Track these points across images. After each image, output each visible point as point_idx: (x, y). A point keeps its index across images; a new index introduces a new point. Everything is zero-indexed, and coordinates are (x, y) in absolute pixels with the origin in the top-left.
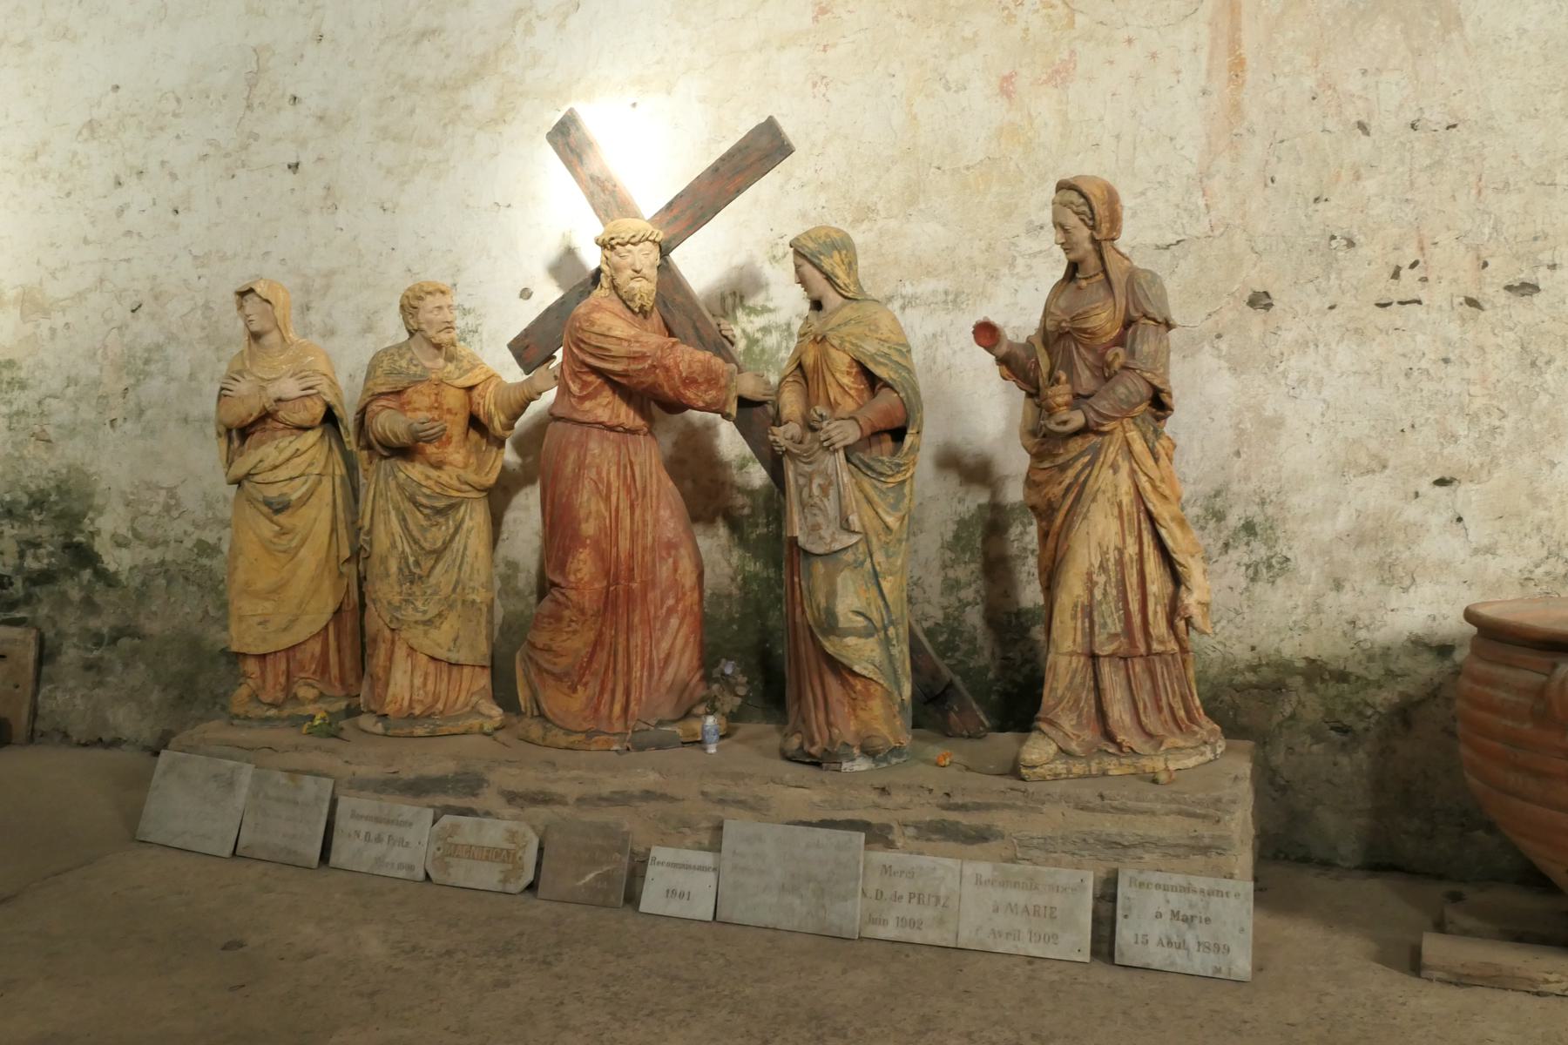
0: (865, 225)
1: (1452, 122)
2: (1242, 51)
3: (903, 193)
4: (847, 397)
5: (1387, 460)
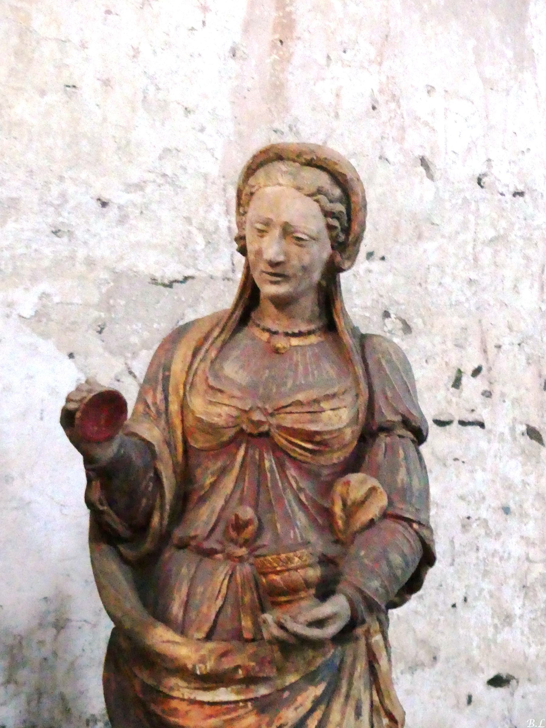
1: (521, 188)
5: (437, 649)
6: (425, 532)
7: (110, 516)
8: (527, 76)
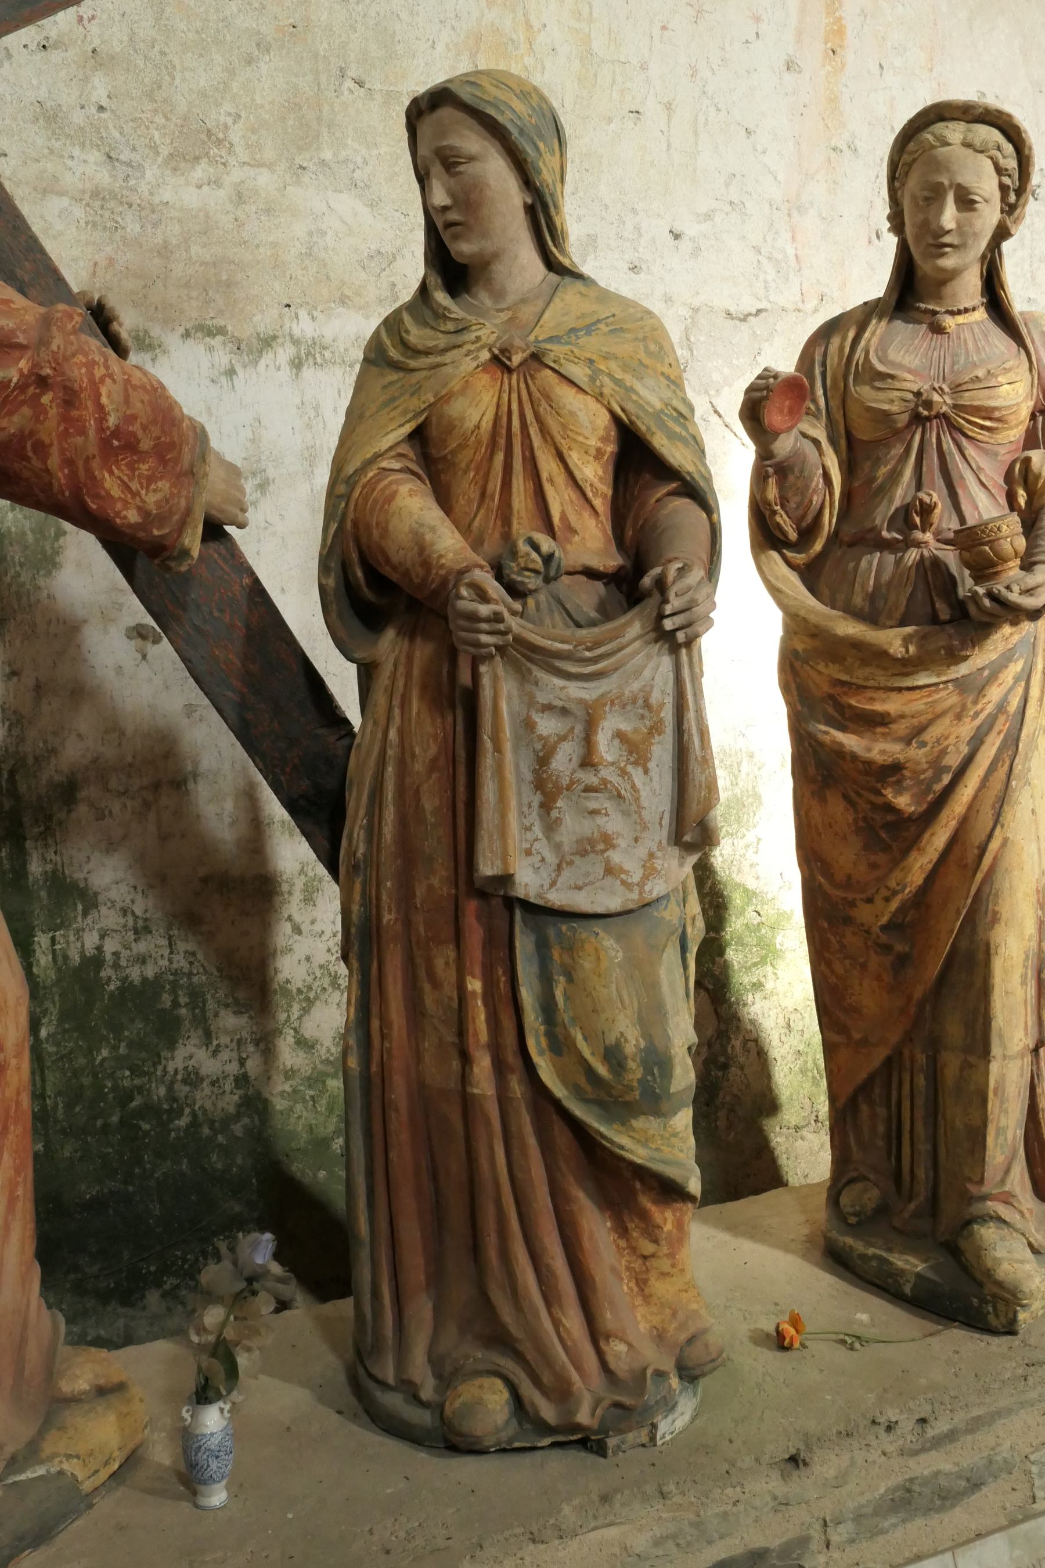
0: (201, 171)
2: (843, 15)
3: (283, 119)
4: (587, 514)
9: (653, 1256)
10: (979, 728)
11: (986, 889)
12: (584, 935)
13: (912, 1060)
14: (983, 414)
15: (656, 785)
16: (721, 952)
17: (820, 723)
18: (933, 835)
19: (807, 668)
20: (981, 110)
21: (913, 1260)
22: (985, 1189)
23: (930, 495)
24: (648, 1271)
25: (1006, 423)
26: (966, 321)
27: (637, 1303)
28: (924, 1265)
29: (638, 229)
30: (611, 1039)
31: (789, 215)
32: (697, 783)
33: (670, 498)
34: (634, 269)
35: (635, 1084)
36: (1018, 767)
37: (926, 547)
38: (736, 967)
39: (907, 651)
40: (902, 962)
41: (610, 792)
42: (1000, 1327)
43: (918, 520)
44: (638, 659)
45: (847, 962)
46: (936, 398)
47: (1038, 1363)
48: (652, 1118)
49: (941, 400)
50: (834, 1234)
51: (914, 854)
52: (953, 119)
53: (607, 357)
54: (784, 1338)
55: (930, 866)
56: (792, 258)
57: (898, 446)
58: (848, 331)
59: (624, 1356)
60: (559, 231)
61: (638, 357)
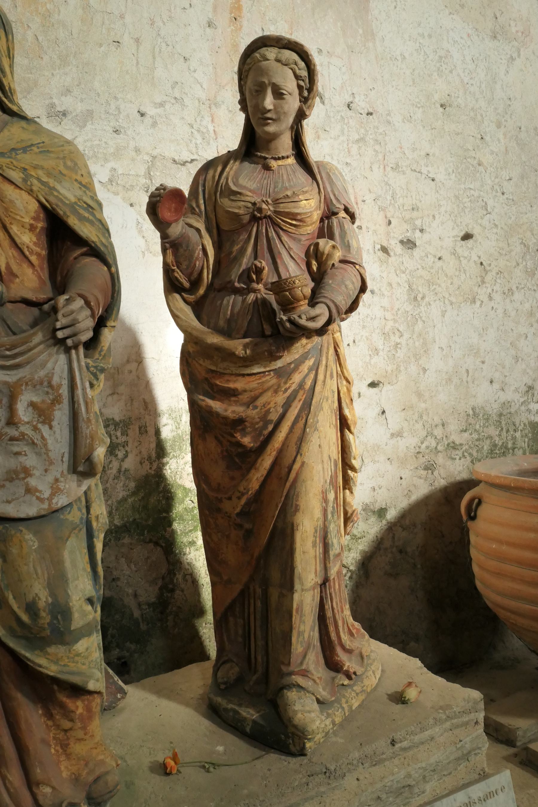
1: (371, 110)
4: (25, 265)
6: (362, 271)
7: (178, 273)
8: (371, 44)
9: (71, 729)
10: (288, 398)
11: (292, 492)
12: (13, 532)
13: (254, 590)
14: (291, 217)
15: (58, 435)
16: (170, 524)
17: (200, 394)
18: (263, 460)
19: (194, 362)
20: (286, 41)
21: (252, 711)
22: (291, 668)
23: (261, 262)
24: (68, 739)
25: (305, 223)
26: (283, 164)
27: (61, 759)
28: (258, 715)
29: (118, 109)
30: (30, 598)
31: (210, 107)
32: (84, 435)
33: (84, 257)
34: (116, 131)
35: (46, 626)
36: (310, 421)
37: (259, 293)
38: (179, 533)
39: (246, 353)
40: (248, 534)
41: (27, 441)
42: (296, 752)
43: (254, 277)
44: (43, 357)
45: (219, 534)
46: (264, 206)
47: (315, 774)
48: (60, 646)
49: (267, 208)
50: (212, 696)
51: (253, 471)
52: (271, 46)
53: (36, 167)
54: (167, 768)
55: (262, 478)
56: (212, 132)
57: (244, 233)
58: (217, 167)
59: (49, 795)
60: (7, 88)
61: (59, 168)
